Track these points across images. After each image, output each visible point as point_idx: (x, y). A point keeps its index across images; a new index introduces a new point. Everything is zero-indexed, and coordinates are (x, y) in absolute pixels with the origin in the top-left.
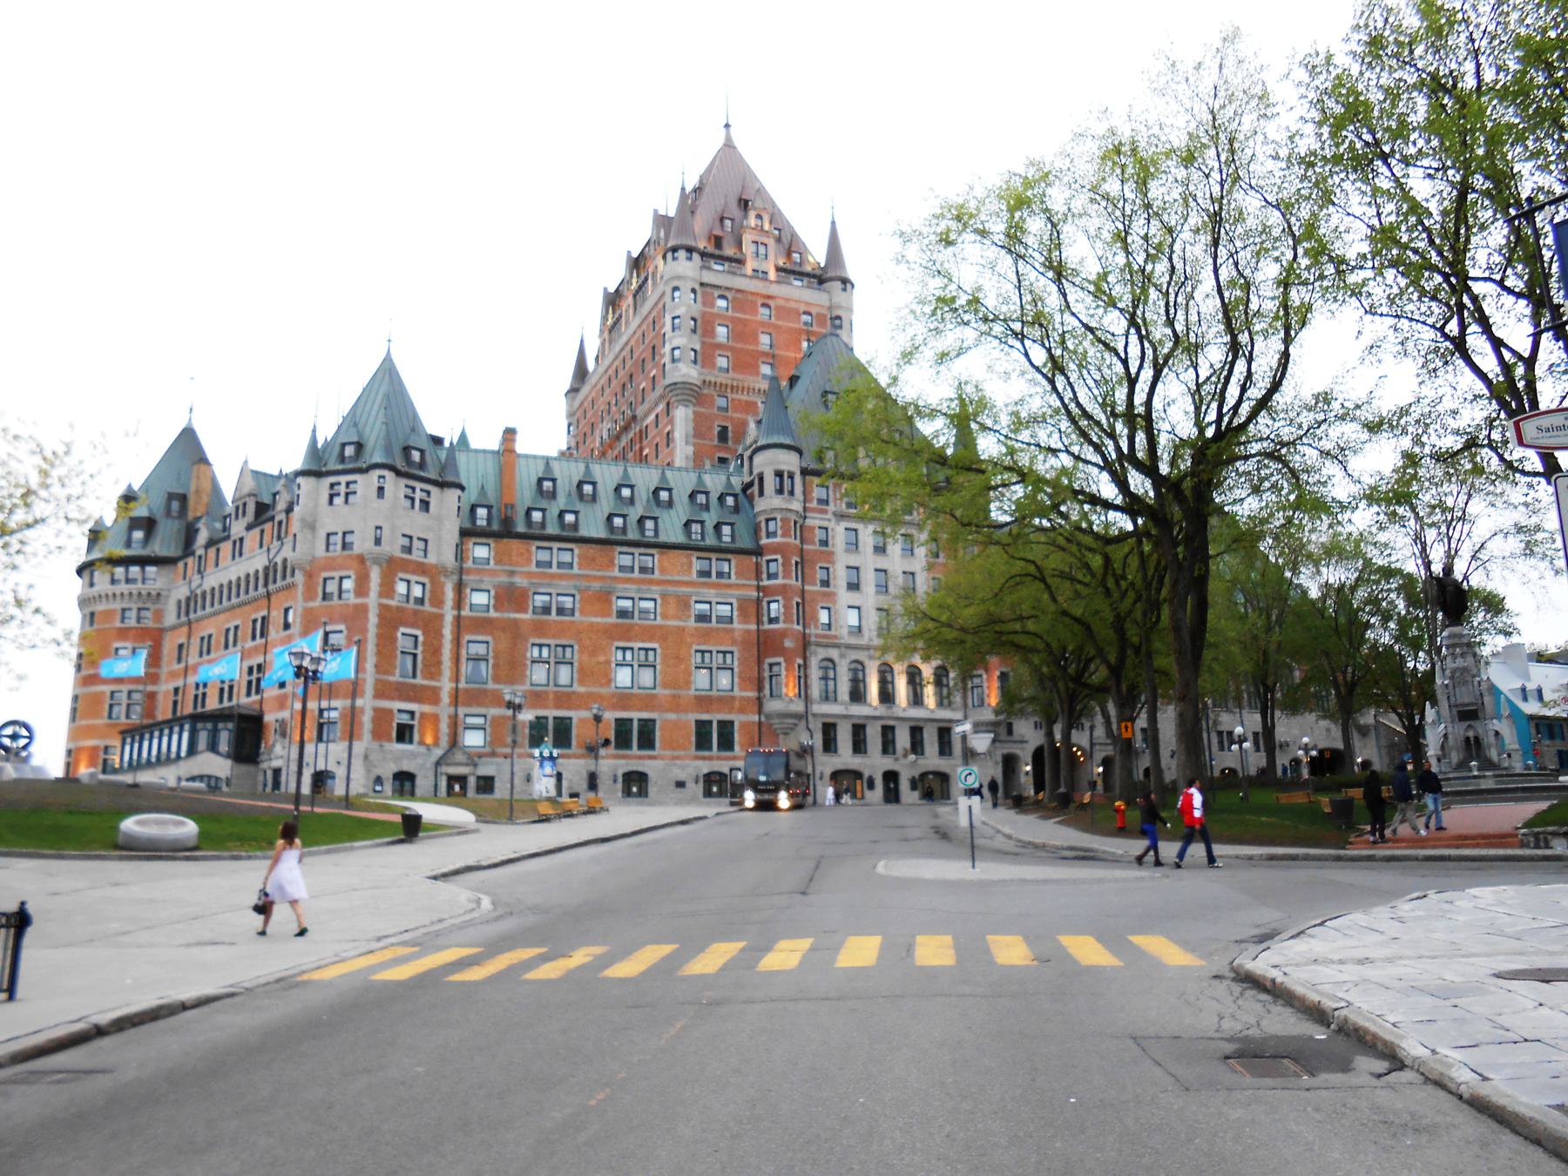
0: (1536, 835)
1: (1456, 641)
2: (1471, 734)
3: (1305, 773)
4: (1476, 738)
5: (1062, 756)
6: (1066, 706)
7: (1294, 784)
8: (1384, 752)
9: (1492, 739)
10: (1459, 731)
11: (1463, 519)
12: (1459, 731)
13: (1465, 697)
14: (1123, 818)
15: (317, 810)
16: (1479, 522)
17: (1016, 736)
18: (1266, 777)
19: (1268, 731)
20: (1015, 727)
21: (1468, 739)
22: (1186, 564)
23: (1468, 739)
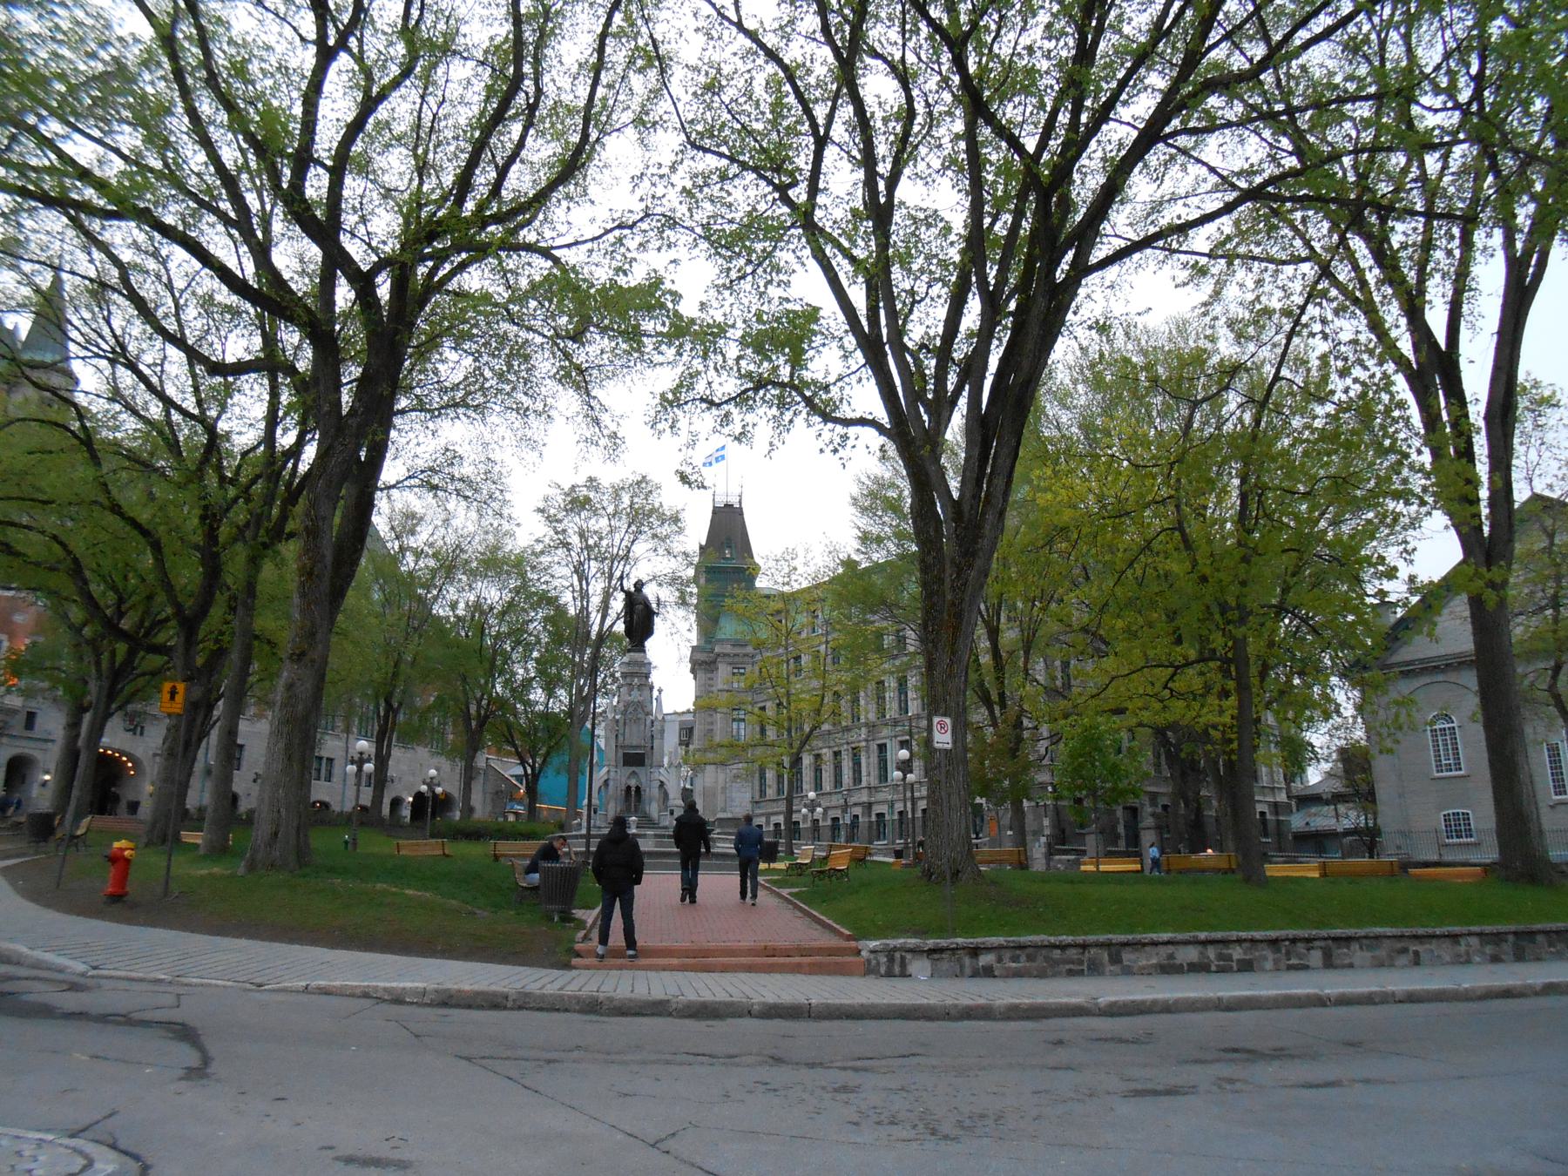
0: (890, 952)
1: (636, 669)
2: (633, 783)
3: (406, 812)
4: (638, 789)
5: (83, 758)
6: (106, 684)
7: (392, 826)
8: (488, 800)
9: (656, 792)
10: (623, 777)
11: (626, 557)
12: (623, 777)
13: (634, 738)
14: (122, 878)
15: (1102, 868)
16: (640, 565)
17: (38, 731)
18: (365, 817)
19: (382, 760)
20: (39, 721)
21: (629, 788)
22: (353, 422)
23: (629, 788)
